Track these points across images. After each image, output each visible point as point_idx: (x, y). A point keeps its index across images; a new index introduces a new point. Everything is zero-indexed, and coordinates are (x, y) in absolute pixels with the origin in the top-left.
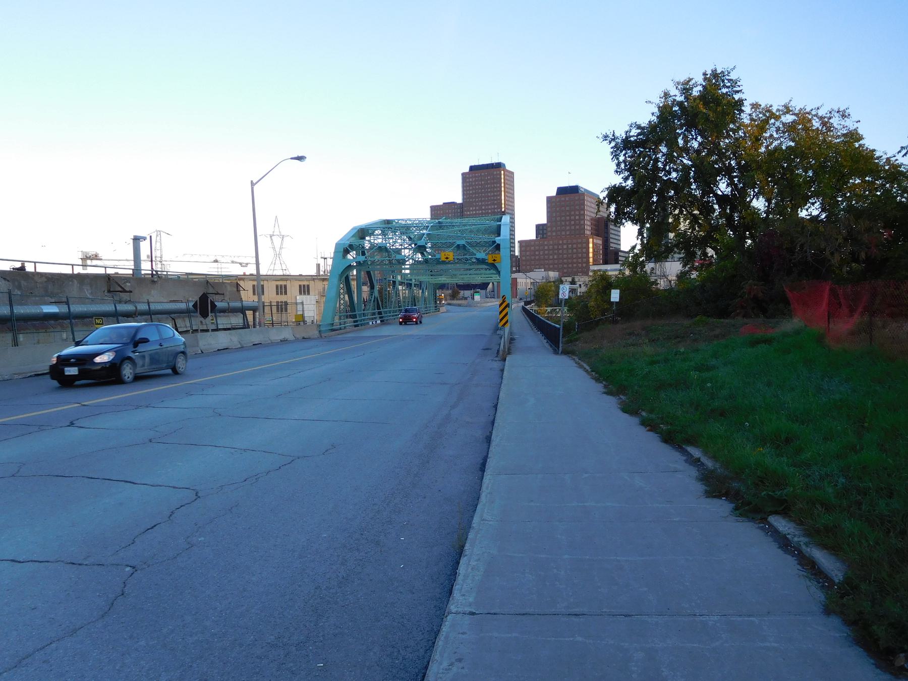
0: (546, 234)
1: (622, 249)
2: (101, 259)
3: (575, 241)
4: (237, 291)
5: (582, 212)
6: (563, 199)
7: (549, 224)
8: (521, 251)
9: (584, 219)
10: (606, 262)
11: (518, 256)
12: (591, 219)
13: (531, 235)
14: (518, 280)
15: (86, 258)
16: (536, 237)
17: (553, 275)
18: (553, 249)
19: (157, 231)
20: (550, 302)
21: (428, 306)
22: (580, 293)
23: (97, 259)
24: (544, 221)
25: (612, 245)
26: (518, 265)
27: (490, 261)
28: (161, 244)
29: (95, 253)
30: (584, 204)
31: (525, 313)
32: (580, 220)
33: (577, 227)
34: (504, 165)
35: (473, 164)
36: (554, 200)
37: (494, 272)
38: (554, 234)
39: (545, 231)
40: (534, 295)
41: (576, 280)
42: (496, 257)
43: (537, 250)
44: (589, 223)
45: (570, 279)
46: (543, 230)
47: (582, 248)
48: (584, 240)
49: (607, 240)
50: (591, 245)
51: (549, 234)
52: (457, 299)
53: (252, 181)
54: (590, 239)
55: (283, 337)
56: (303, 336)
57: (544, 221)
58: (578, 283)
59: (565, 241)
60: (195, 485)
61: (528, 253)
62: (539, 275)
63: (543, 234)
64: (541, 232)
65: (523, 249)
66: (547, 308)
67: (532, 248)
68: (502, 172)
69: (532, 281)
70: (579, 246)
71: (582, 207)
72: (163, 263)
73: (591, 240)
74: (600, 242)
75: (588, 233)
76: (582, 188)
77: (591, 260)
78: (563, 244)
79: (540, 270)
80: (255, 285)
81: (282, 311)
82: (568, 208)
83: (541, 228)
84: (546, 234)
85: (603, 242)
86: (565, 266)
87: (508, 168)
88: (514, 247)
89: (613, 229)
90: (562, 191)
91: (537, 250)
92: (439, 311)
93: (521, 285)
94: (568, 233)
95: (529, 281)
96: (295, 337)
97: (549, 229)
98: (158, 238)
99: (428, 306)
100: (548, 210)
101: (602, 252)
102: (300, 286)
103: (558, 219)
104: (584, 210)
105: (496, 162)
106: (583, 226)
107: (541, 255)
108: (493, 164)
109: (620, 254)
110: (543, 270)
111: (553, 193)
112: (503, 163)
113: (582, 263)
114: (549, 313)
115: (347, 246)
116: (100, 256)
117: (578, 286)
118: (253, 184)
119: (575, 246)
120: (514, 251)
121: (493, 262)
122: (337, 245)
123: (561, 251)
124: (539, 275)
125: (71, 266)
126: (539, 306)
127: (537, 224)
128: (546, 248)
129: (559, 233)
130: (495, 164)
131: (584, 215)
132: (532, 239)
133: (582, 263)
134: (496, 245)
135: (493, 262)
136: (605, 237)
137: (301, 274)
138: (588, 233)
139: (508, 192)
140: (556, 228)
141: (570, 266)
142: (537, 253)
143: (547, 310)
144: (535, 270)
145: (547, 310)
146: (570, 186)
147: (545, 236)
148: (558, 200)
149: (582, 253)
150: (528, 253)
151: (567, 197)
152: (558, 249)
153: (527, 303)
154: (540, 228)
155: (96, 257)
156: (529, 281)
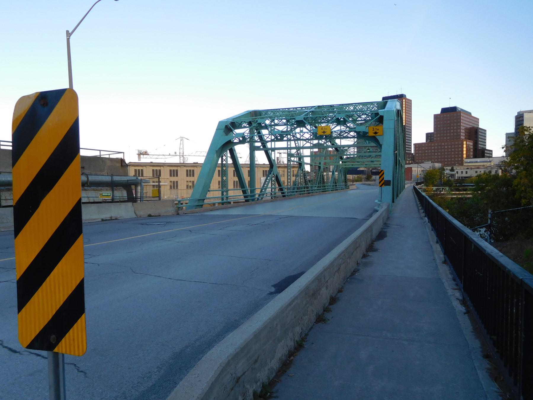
0: (433, 139)
1: (487, 148)
2: (148, 155)
3: (453, 143)
4: (122, 166)
5: (459, 124)
6: (445, 116)
7: (435, 133)
8: (415, 150)
9: (460, 129)
10: (475, 157)
11: (413, 154)
12: (465, 129)
13: (423, 140)
14: (413, 169)
15: (140, 154)
16: (426, 141)
17: (438, 165)
18: (438, 149)
19: (181, 137)
20: (436, 183)
21: (337, 184)
22: (457, 177)
23: (146, 155)
24: (431, 130)
25: (480, 146)
26: (414, 159)
27: (371, 134)
28: (183, 145)
29: (145, 151)
30: (460, 119)
31: (415, 191)
32: (457, 129)
33: (455, 134)
34: (405, 96)
35: (385, 96)
36: (439, 117)
37: (374, 145)
38: (439, 139)
39: (432, 138)
40: (424, 178)
41: (455, 168)
42: (378, 129)
43: (427, 150)
44: (463, 131)
45: (450, 168)
46: (431, 136)
47: (458, 148)
48: (460, 143)
49: (476, 142)
50: (465, 146)
51: (435, 139)
52: (370, 181)
53: (67, 31)
54: (464, 142)
55: (110, 216)
56: (149, 213)
57: (431, 130)
58: (456, 171)
59: (446, 144)
60: (252, 271)
61: (420, 152)
62: (427, 165)
63: (431, 139)
64: (429, 138)
65: (417, 149)
66: (433, 188)
67: (424, 148)
68: (404, 100)
69: (422, 169)
70: (456, 146)
71: (459, 120)
72: (184, 157)
73: (465, 142)
74: (472, 144)
75: (463, 138)
76: (459, 108)
77: (465, 156)
78: (444, 146)
79: (428, 162)
80: (220, 170)
81: (174, 188)
82: (449, 122)
83: (429, 135)
84: (433, 139)
85: (473, 144)
86: (446, 160)
87: (407, 97)
88: (411, 148)
89: (481, 135)
90: (444, 111)
91: (427, 150)
92: (348, 189)
93: (415, 172)
94: (448, 138)
95: (419, 169)
96: (136, 215)
97: (435, 136)
98: (182, 142)
99: (337, 184)
100: (435, 127)
101: (473, 150)
102: (263, 171)
103: (442, 129)
104: (460, 122)
105: (400, 94)
106: (459, 133)
107: (429, 153)
108: (398, 95)
109: (486, 152)
110: (430, 162)
111: (439, 112)
112: (404, 95)
113: (458, 158)
114: (434, 191)
115: (228, 124)
116: (148, 152)
117: (456, 172)
118: (69, 34)
119: (453, 146)
120: (411, 151)
121: (374, 135)
122: (220, 123)
123: (443, 150)
124: (427, 165)
125: (108, 155)
126: (427, 186)
127: (427, 132)
128: (433, 148)
129: (442, 138)
130: (399, 95)
131: (460, 126)
132: (423, 142)
133: (458, 158)
134: (378, 118)
135: (374, 135)
136: (475, 141)
137: (264, 163)
138: (463, 138)
139: (407, 113)
140: (440, 135)
141: (450, 160)
142: (426, 151)
143: (433, 189)
144: (424, 162)
145: (433, 189)
146: (450, 107)
147: (432, 140)
148: (442, 116)
149: (458, 151)
150: (420, 152)
151: (448, 115)
152: (441, 149)
153: (418, 184)
154: (428, 136)
155: (146, 153)
156: (419, 169)
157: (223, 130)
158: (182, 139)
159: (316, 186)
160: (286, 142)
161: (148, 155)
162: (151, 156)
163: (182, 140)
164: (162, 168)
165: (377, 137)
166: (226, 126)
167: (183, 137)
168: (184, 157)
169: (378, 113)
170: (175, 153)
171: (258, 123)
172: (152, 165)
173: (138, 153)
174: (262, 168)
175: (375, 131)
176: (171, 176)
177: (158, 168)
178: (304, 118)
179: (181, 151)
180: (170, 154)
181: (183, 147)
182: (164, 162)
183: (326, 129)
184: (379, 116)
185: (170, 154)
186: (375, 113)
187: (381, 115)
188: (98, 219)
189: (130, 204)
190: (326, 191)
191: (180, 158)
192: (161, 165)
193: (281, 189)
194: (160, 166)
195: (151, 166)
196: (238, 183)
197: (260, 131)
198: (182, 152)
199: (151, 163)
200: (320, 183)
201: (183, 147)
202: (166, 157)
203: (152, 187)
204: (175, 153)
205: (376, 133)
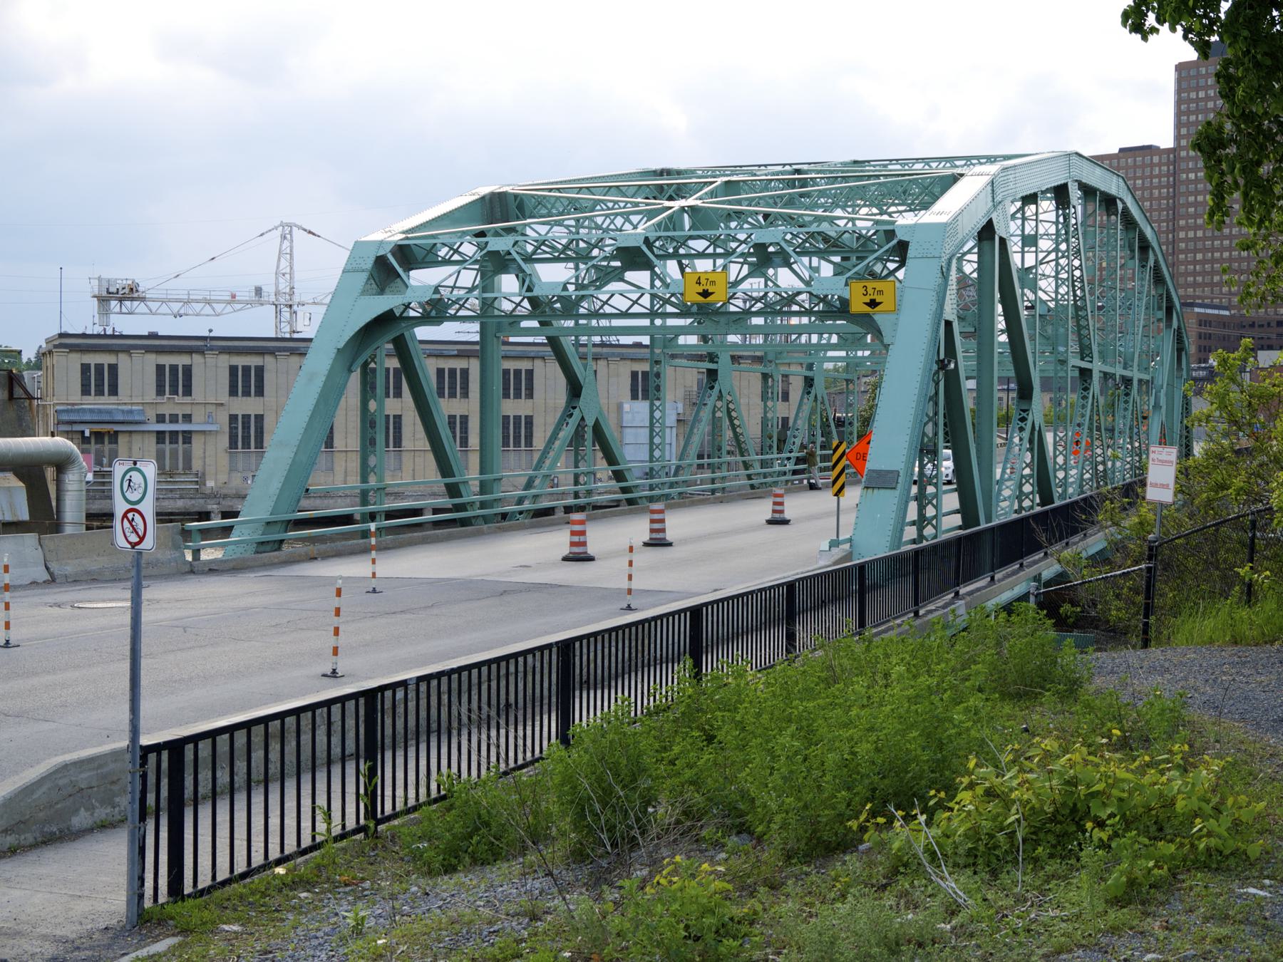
2: (143, 299)
19: (283, 225)
29: (130, 282)
42: (881, 292)
81: (246, 444)
98: (286, 243)
116: (140, 289)
135: (868, 309)
155: (130, 294)
157: (365, 276)
158: (287, 231)
159: (789, 459)
160: (712, 261)
161: (143, 299)
162: (154, 306)
163: (288, 236)
164: (197, 359)
165: (876, 317)
166: (381, 262)
167: (290, 226)
168: (295, 308)
169: (893, 231)
170: (258, 291)
171: (489, 252)
172: (154, 344)
173: (97, 293)
174: (628, 362)
175: (872, 297)
176: (233, 392)
177: (181, 360)
178: (647, 240)
179: (283, 286)
180: (234, 296)
181: (291, 268)
182: (206, 334)
183: (713, 283)
184: (894, 242)
185: (234, 296)
186: (885, 231)
187: (902, 238)
188: (1003, 579)
189: (30, 539)
190: (464, 522)
191: (278, 313)
192: (190, 347)
193: (619, 476)
194: (190, 351)
195: (149, 350)
196: (520, 428)
197: (407, 335)
198: (287, 290)
199: (153, 336)
200: (771, 447)
201: (291, 268)
202: (219, 307)
203: (153, 439)
204: (258, 291)
205: (873, 304)
